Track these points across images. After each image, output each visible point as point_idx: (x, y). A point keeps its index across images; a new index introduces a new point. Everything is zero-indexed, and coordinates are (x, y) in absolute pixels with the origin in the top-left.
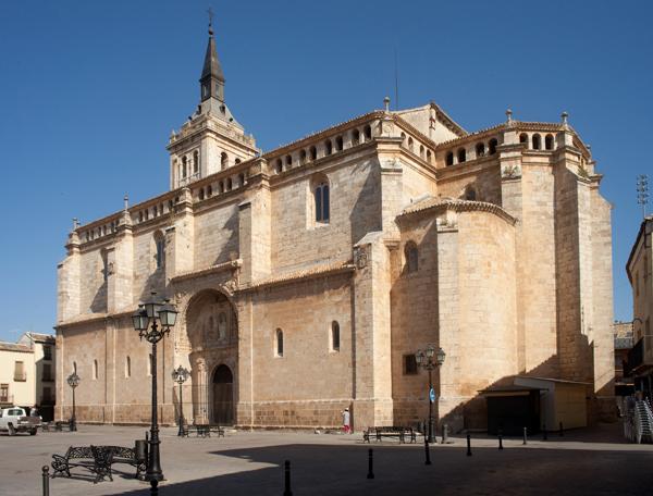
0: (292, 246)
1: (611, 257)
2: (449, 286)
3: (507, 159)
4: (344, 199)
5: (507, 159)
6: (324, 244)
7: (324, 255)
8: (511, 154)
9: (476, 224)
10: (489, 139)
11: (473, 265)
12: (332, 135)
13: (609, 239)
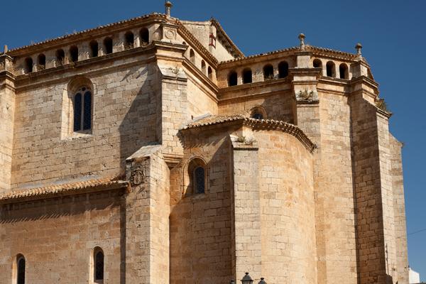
0: (42, 158)
1: (403, 196)
2: (247, 211)
3: (302, 83)
4: (112, 107)
5: (302, 83)
6: (83, 158)
7: (84, 169)
8: (305, 78)
9: (276, 145)
10: (279, 62)
11: (272, 189)
12: (99, 37)
13: (401, 178)
